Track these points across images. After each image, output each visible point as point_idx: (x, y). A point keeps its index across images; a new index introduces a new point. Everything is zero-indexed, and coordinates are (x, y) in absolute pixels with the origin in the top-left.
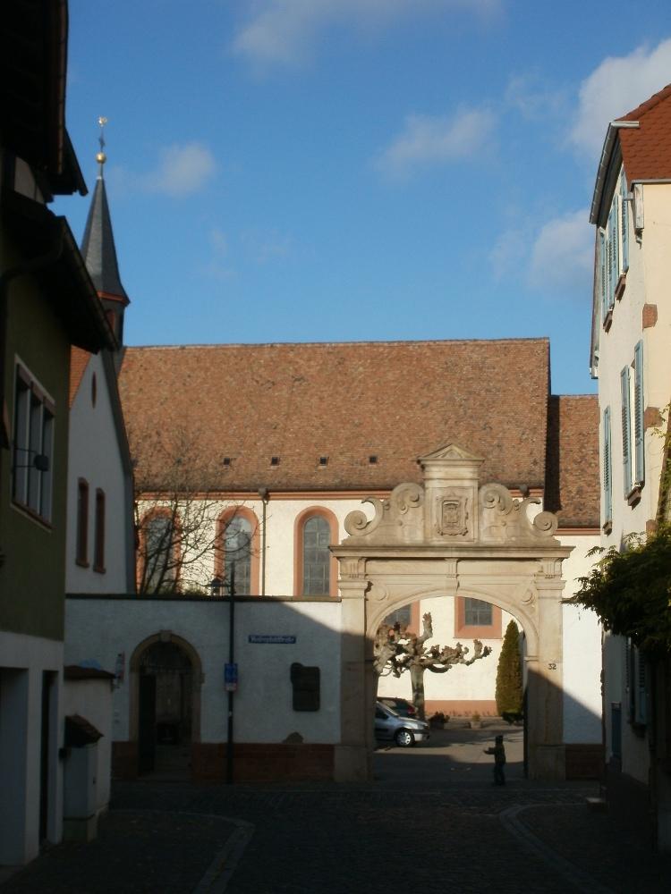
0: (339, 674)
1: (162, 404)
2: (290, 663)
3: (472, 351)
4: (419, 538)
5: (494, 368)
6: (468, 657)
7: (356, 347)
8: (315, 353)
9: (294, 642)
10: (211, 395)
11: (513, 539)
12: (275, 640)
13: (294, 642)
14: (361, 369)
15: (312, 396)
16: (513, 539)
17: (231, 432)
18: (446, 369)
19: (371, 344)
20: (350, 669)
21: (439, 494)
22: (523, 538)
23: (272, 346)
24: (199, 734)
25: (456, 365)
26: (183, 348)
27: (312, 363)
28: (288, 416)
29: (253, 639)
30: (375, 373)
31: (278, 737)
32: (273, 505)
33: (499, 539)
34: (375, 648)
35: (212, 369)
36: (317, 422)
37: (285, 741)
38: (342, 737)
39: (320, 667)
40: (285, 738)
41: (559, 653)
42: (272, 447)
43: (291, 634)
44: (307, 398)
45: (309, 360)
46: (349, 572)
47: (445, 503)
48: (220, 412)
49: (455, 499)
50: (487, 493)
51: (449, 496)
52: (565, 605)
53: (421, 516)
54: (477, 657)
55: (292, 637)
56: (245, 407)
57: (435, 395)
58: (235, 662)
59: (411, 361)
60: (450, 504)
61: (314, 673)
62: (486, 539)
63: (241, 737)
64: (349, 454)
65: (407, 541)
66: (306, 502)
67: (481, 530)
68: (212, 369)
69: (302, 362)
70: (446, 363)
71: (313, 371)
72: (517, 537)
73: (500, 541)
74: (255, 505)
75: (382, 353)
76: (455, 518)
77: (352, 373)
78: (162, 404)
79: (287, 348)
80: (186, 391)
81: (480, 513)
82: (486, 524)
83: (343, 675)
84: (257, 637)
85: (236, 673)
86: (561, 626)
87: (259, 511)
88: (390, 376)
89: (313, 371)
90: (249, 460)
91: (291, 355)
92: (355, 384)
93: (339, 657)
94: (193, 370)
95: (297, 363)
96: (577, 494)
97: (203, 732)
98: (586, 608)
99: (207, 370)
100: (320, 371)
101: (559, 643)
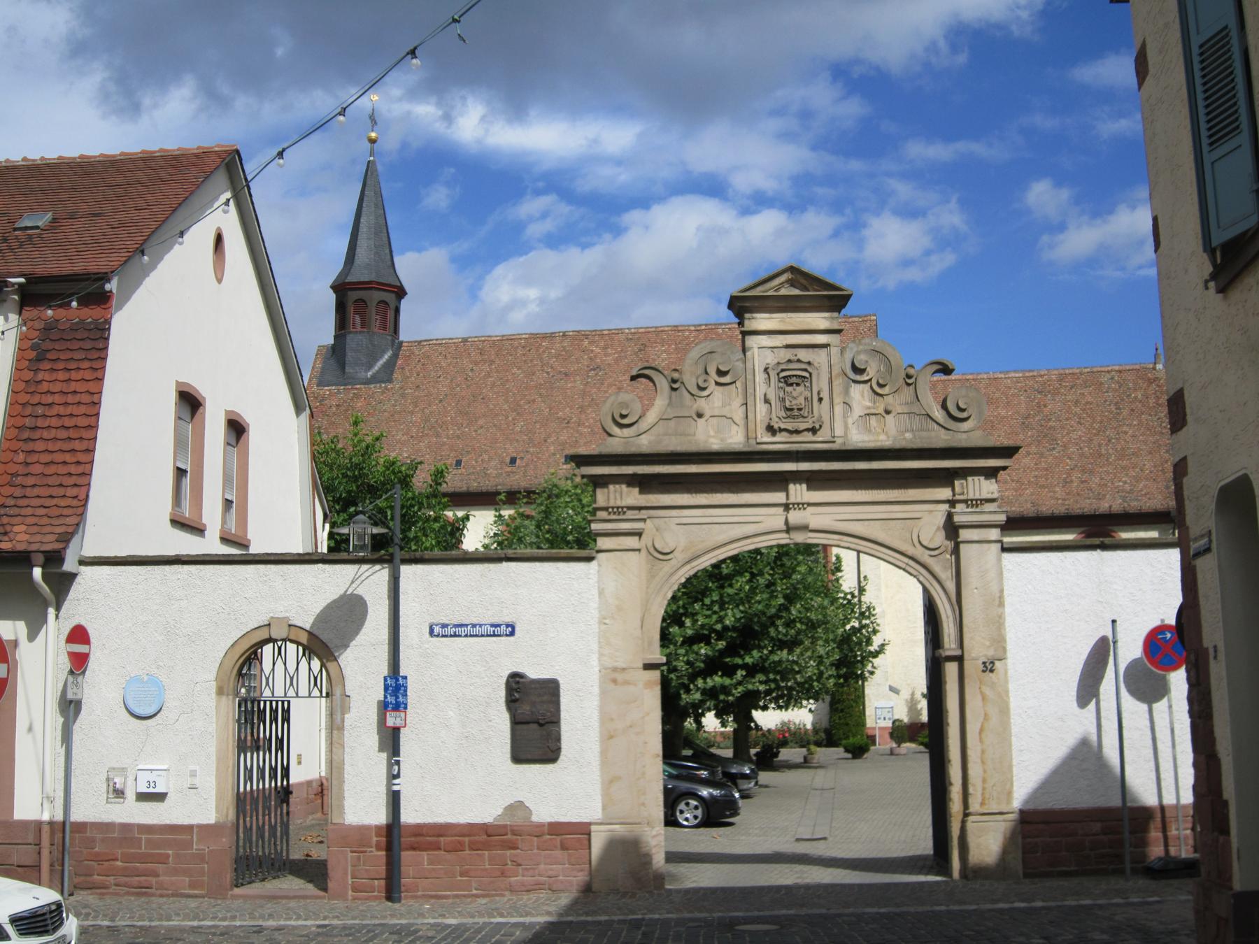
0: (596, 690)
1: (441, 401)
2: (507, 673)
4: (735, 439)
7: (658, 332)
8: (612, 339)
9: (512, 634)
10: (495, 389)
11: (908, 435)
12: (477, 630)
13: (512, 634)
14: (664, 355)
15: (610, 385)
16: (908, 435)
17: (518, 429)
19: (676, 328)
20: (615, 681)
21: (771, 359)
22: (924, 434)
23: (564, 335)
24: (341, 807)
26: (465, 340)
27: (609, 351)
28: (582, 409)
29: (437, 630)
31: (485, 812)
33: (883, 437)
38: (604, 808)
39: (509, 761)
40: (500, 811)
41: (999, 641)
42: (564, 444)
43: (508, 620)
44: (604, 388)
45: (605, 348)
46: (612, 504)
47: (783, 374)
48: (506, 407)
49: (803, 366)
50: (858, 353)
51: (789, 361)
52: (1006, 556)
53: (738, 401)
55: (508, 626)
56: (534, 401)
58: (403, 672)
60: (792, 377)
61: (551, 689)
62: (858, 438)
63: (409, 816)
65: (715, 445)
67: (850, 421)
69: (598, 350)
71: (610, 360)
72: (912, 431)
73: (882, 440)
75: (688, 338)
76: (801, 400)
78: (441, 401)
79: (581, 335)
80: (468, 387)
81: (846, 392)
82: (858, 411)
83: (604, 693)
84: (444, 626)
85: (405, 695)
86: (1002, 591)
89: (610, 360)
90: (539, 458)
91: (586, 343)
93: (594, 661)
94: (476, 363)
97: (349, 803)
99: (492, 362)
100: (617, 360)
101: (999, 622)
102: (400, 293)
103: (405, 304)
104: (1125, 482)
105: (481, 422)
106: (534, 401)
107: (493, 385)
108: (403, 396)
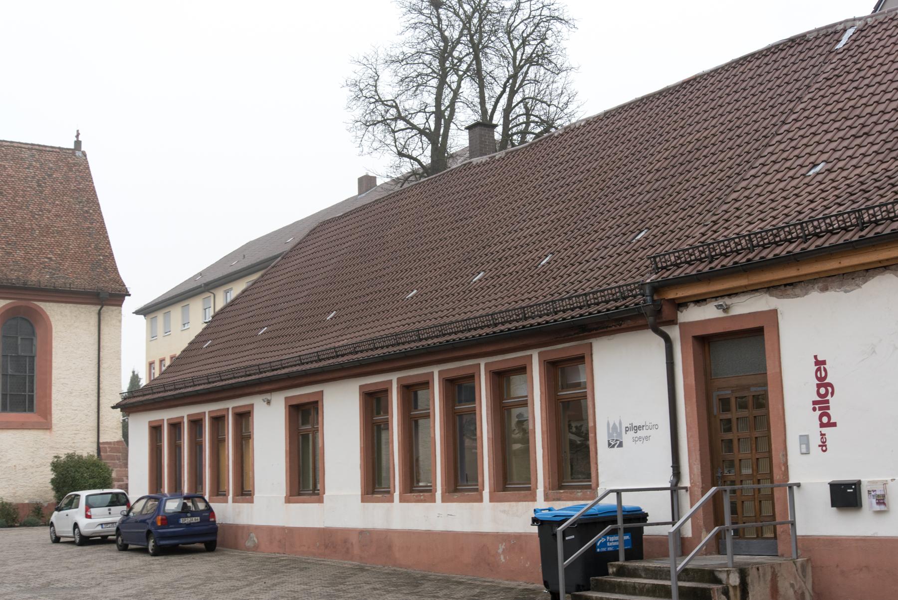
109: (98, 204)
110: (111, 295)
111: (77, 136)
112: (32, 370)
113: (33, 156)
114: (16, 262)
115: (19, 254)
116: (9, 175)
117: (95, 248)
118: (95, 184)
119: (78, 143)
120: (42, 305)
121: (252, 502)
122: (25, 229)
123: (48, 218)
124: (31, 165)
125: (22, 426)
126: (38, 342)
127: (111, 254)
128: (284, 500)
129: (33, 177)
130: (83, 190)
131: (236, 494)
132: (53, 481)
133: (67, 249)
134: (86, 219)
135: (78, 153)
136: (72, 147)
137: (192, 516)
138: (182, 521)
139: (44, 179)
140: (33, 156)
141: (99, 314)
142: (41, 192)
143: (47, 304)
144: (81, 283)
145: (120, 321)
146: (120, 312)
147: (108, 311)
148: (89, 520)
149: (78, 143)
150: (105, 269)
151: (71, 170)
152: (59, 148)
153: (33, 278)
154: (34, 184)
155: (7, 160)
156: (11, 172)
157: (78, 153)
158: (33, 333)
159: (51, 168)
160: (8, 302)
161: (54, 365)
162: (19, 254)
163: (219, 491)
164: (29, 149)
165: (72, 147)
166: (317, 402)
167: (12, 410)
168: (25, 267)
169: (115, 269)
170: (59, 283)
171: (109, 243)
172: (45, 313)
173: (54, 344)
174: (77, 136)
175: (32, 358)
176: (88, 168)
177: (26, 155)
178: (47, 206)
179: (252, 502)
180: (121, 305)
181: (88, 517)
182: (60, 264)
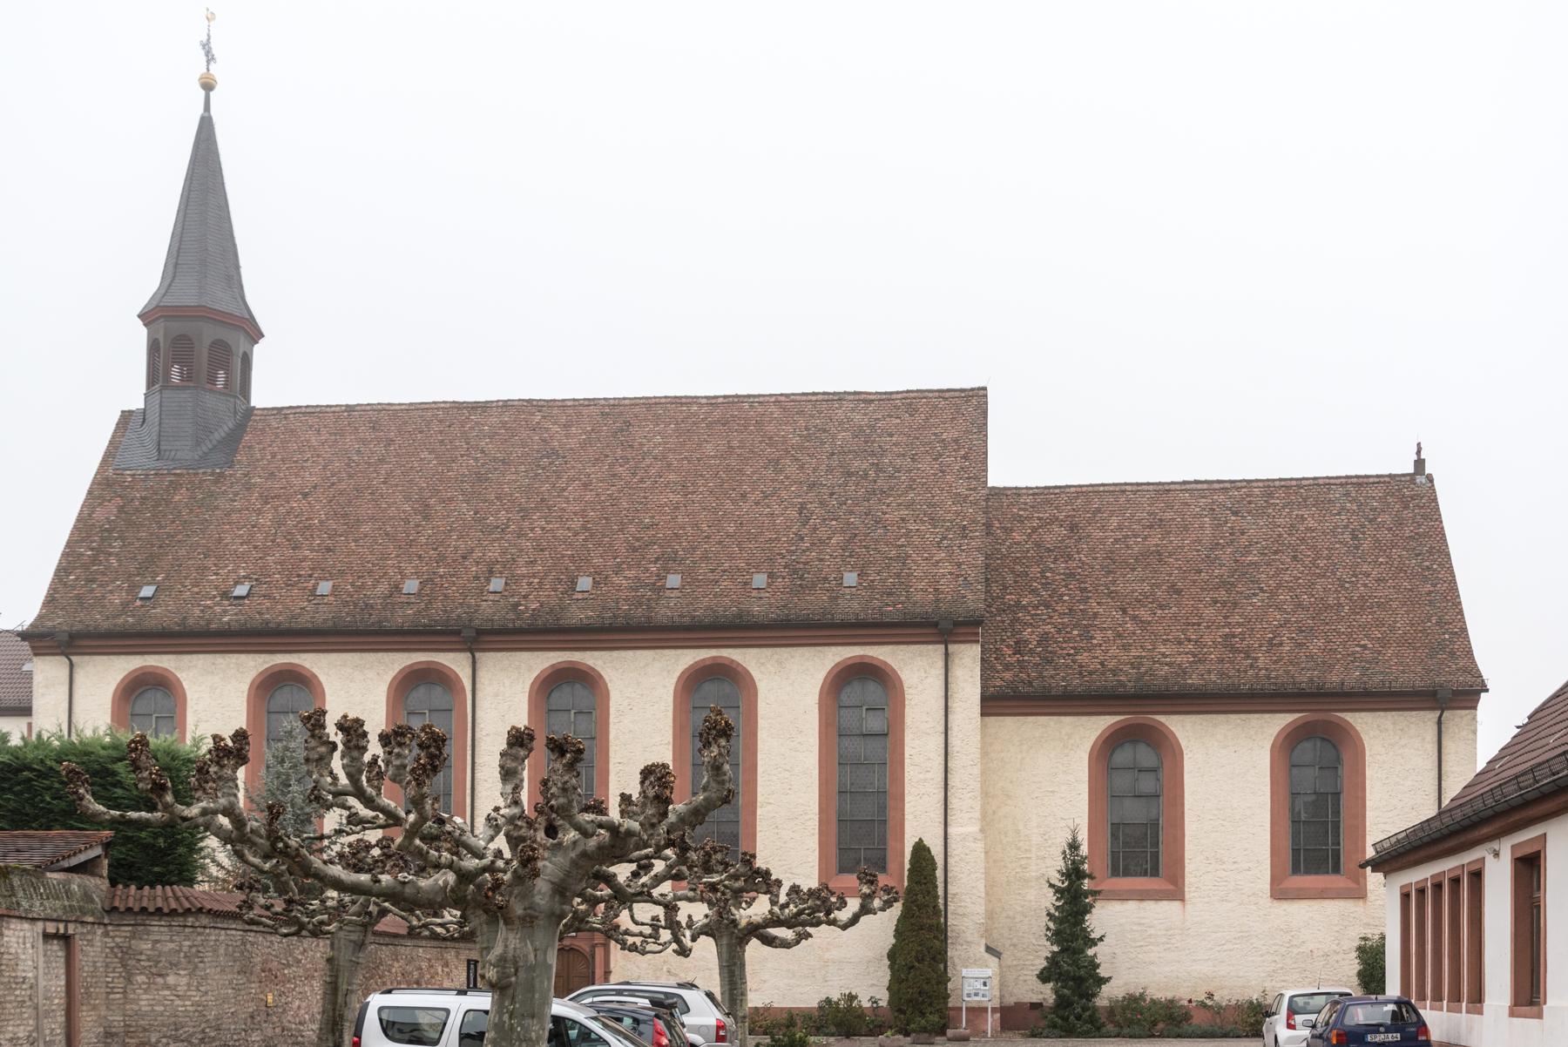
3: (853, 410)
5: (891, 435)
6: (843, 915)
18: (808, 438)
25: (825, 431)
30: (683, 444)
32: (488, 660)
34: (1083, 837)
35: (399, 441)
36: (576, 524)
37: (40, 617)
54: (865, 910)
57: (787, 478)
59: (746, 427)
64: (631, 574)
66: (552, 654)
68: (399, 441)
69: (556, 428)
70: (807, 429)
71: (573, 443)
74: (456, 663)
75: (695, 414)
77: (641, 444)
80: (350, 476)
87: (465, 676)
88: (709, 449)
89: (429, 823)
92: (648, 462)
95: (547, 430)
96: (1039, 644)
98: (1058, 890)
100: (583, 445)
102: (255, 335)
103: (259, 352)
104: (1364, 647)
105: (365, 528)
106: (451, 499)
107: (389, 474)
108: (249, 488)
109: (1448, 554)
110: (1456, 693)
111: (1419, 452)
112: (1337, 813)
113: (1347, 494)
114: (1311, 657)
115: (1316, 645)
116: (1309, 529)
117: (1438, 624)
118: (1445, 524)
119: (1420, 464)
120: (1349, 717)
121: (1540, 1016)
122: (1328, 607)
123: (1365, 585)
124: (1343, 508)
125: (1143, 896)
126: (1345, 771)
127: (1464, 630)
128: (1507, 1012)
129: (1346, 527)
130: (1425, 535)
131: (1471, 1001)
132: (1360, 974)
133: (1392, 629)
134: (1425, 579)
135: (1420, 479)
136: (1411, 471)
137: (1387, 1032)
138: (1369, 1038)
139: (1363, 526)
140: (1347, 494)
141: (1439, 723)
142: (1357, 548)
143: (1176, 717)
144: (1411, 676)
145: (1475, 732)
146: (1474, 718)
147: (1453, 718)
148: (1292, 1032)
149: (1420, 464)
150: (1452, 653)
151: (1406, 507)
152: (1390, 476)
153: (1334, 679)
154: (1347, 536)
155: (1306, 506)
156: (1311, 523)
157: (1420, 479)
158: (1338, 759)
159: (1373, 509)
160: (1297, 716)
161: (1368, 803)
162: (1316, 645)
163: (1422, 997)
164: (1341, 485)
165: (1411, 471)
166: (1539, 852)
167: (1307, 872)
168: (1324, 663)
169: (1469, 653)
170: (1375, 681)
171: (1461, 612)
172: (1353, 728)
173: (1370, 773)
174: (1419, 452)
175: (1337, 795)
176: (1435, 500)
177: (1337, 493)
178: (1365, 568)
179: (1540, 1016)
180: (1475, 708)
181: (1291, 1026)
182: (1379, 653)
